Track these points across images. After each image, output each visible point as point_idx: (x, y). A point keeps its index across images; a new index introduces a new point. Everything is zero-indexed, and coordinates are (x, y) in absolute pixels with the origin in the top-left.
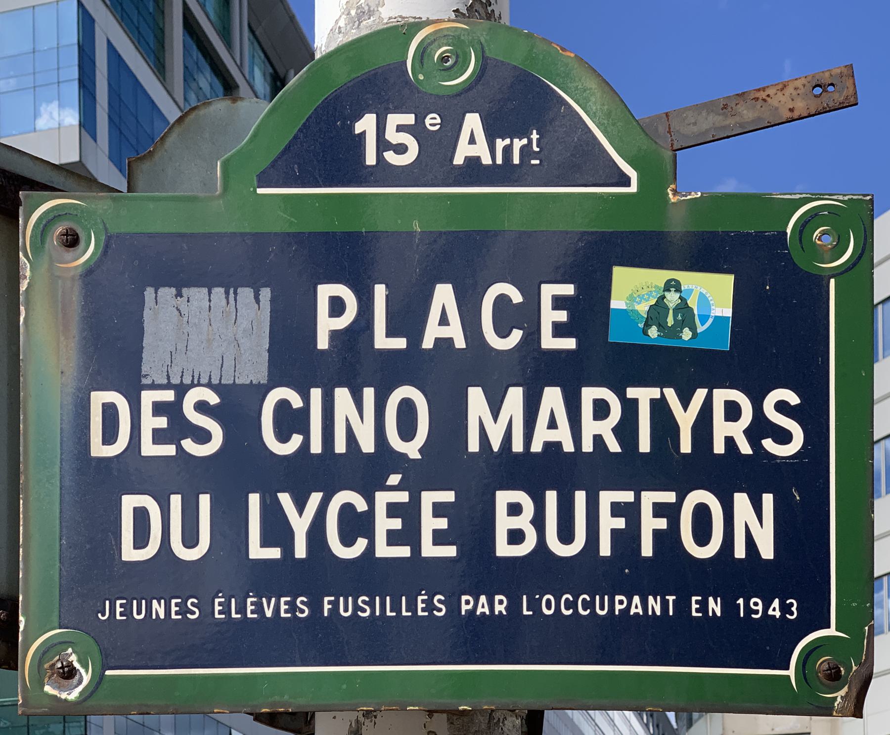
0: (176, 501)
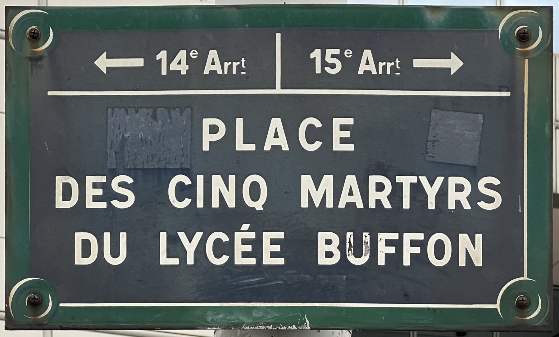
0: (107, 236)
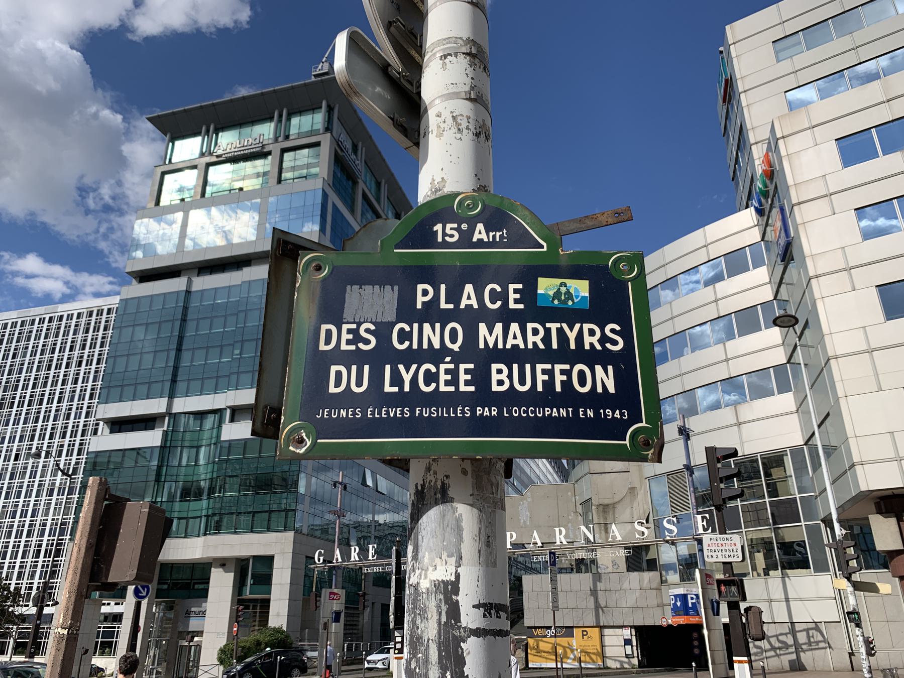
0: (354, 368)
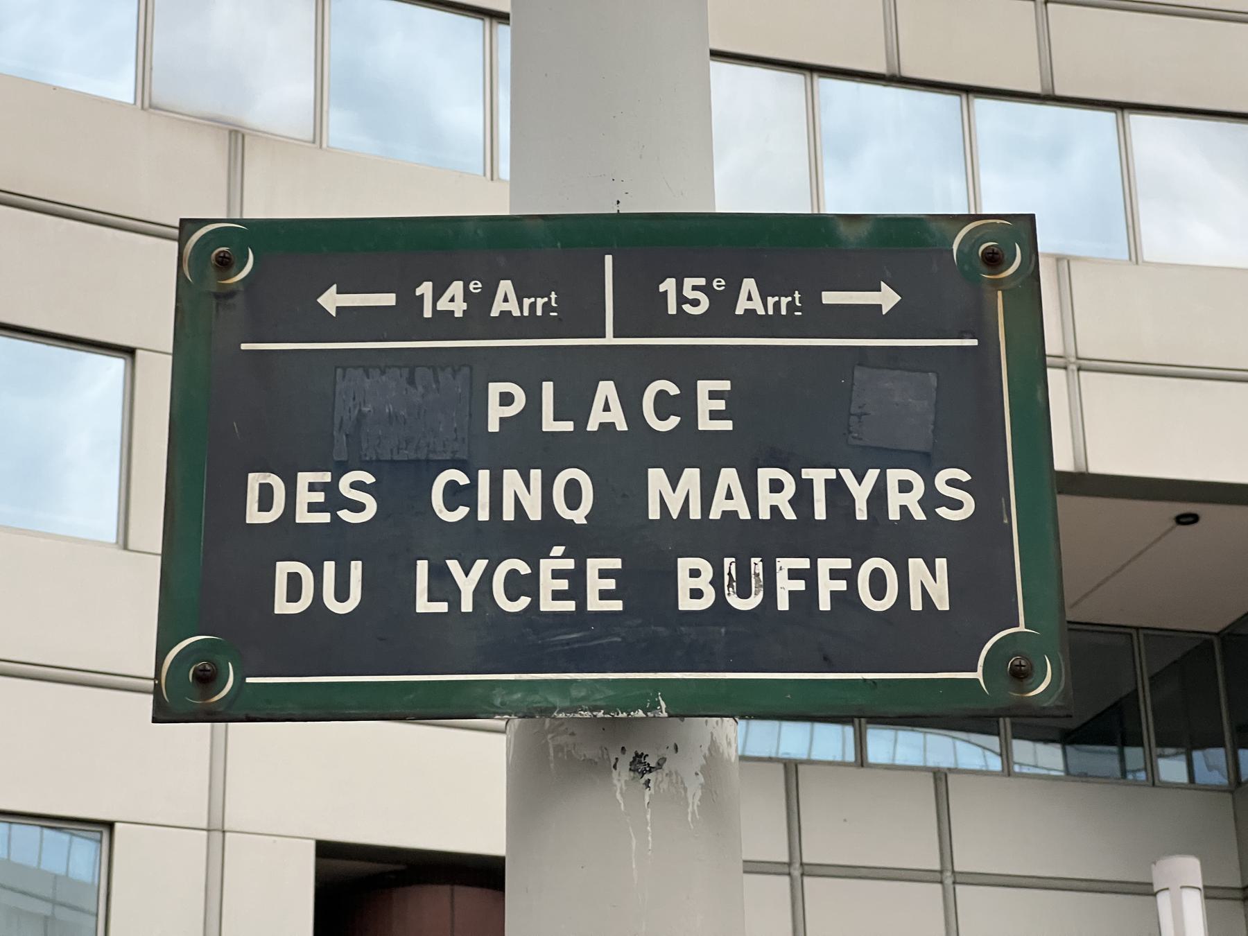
0: (329, 568)
